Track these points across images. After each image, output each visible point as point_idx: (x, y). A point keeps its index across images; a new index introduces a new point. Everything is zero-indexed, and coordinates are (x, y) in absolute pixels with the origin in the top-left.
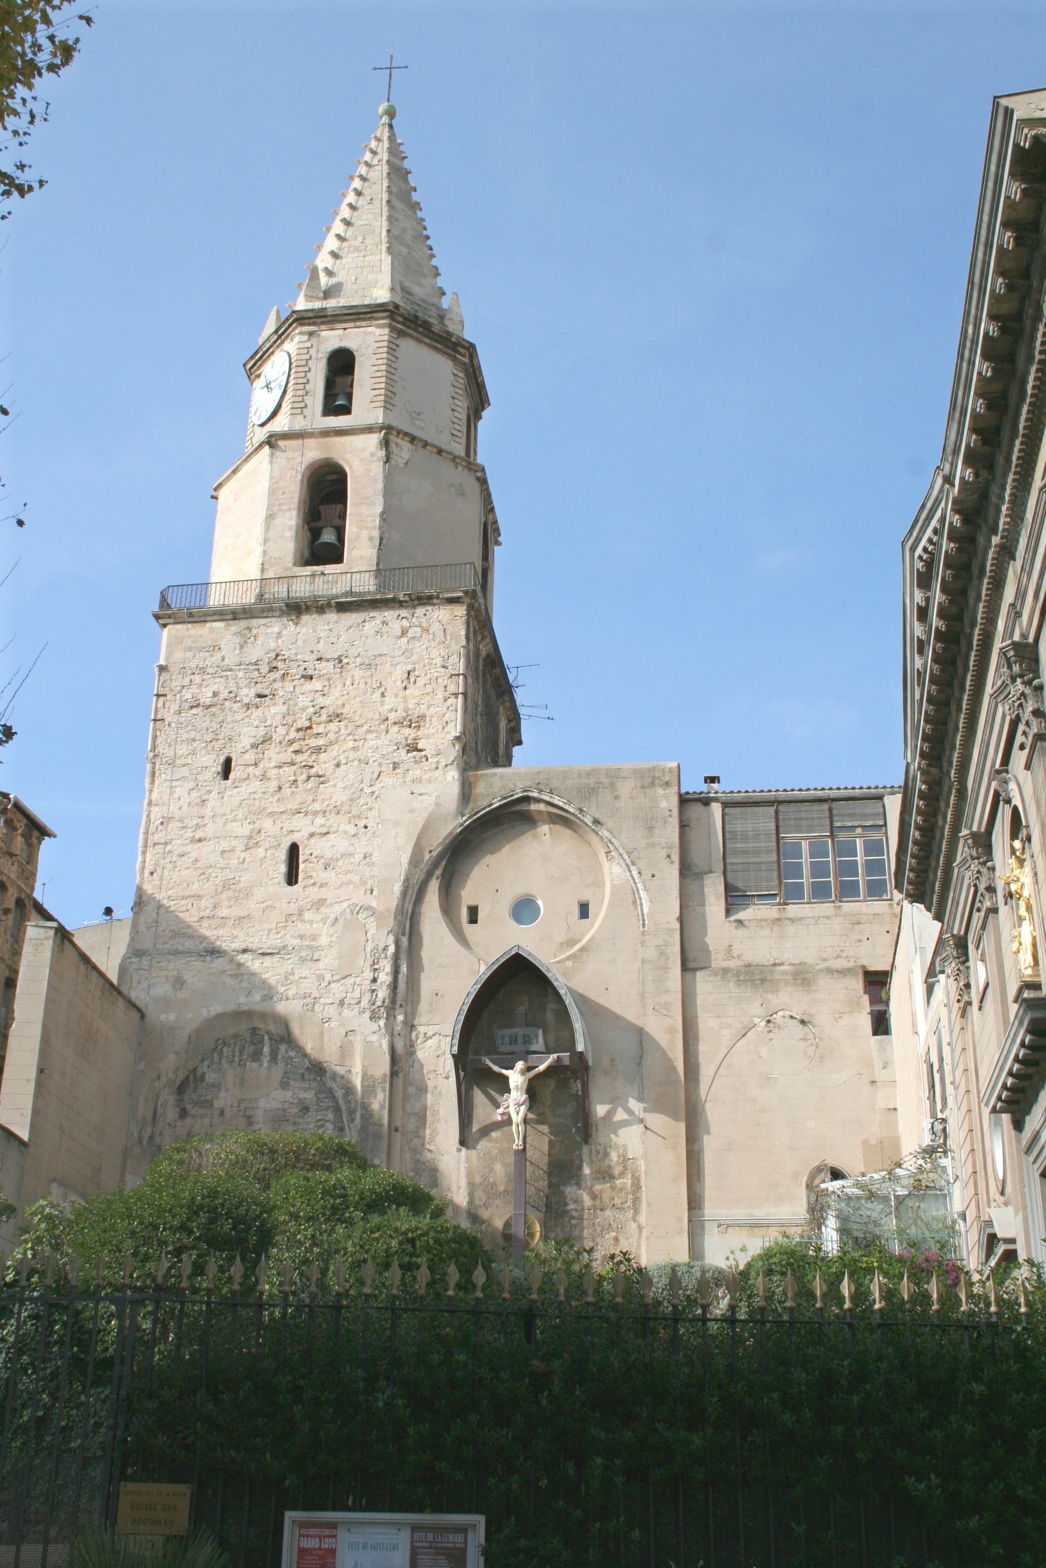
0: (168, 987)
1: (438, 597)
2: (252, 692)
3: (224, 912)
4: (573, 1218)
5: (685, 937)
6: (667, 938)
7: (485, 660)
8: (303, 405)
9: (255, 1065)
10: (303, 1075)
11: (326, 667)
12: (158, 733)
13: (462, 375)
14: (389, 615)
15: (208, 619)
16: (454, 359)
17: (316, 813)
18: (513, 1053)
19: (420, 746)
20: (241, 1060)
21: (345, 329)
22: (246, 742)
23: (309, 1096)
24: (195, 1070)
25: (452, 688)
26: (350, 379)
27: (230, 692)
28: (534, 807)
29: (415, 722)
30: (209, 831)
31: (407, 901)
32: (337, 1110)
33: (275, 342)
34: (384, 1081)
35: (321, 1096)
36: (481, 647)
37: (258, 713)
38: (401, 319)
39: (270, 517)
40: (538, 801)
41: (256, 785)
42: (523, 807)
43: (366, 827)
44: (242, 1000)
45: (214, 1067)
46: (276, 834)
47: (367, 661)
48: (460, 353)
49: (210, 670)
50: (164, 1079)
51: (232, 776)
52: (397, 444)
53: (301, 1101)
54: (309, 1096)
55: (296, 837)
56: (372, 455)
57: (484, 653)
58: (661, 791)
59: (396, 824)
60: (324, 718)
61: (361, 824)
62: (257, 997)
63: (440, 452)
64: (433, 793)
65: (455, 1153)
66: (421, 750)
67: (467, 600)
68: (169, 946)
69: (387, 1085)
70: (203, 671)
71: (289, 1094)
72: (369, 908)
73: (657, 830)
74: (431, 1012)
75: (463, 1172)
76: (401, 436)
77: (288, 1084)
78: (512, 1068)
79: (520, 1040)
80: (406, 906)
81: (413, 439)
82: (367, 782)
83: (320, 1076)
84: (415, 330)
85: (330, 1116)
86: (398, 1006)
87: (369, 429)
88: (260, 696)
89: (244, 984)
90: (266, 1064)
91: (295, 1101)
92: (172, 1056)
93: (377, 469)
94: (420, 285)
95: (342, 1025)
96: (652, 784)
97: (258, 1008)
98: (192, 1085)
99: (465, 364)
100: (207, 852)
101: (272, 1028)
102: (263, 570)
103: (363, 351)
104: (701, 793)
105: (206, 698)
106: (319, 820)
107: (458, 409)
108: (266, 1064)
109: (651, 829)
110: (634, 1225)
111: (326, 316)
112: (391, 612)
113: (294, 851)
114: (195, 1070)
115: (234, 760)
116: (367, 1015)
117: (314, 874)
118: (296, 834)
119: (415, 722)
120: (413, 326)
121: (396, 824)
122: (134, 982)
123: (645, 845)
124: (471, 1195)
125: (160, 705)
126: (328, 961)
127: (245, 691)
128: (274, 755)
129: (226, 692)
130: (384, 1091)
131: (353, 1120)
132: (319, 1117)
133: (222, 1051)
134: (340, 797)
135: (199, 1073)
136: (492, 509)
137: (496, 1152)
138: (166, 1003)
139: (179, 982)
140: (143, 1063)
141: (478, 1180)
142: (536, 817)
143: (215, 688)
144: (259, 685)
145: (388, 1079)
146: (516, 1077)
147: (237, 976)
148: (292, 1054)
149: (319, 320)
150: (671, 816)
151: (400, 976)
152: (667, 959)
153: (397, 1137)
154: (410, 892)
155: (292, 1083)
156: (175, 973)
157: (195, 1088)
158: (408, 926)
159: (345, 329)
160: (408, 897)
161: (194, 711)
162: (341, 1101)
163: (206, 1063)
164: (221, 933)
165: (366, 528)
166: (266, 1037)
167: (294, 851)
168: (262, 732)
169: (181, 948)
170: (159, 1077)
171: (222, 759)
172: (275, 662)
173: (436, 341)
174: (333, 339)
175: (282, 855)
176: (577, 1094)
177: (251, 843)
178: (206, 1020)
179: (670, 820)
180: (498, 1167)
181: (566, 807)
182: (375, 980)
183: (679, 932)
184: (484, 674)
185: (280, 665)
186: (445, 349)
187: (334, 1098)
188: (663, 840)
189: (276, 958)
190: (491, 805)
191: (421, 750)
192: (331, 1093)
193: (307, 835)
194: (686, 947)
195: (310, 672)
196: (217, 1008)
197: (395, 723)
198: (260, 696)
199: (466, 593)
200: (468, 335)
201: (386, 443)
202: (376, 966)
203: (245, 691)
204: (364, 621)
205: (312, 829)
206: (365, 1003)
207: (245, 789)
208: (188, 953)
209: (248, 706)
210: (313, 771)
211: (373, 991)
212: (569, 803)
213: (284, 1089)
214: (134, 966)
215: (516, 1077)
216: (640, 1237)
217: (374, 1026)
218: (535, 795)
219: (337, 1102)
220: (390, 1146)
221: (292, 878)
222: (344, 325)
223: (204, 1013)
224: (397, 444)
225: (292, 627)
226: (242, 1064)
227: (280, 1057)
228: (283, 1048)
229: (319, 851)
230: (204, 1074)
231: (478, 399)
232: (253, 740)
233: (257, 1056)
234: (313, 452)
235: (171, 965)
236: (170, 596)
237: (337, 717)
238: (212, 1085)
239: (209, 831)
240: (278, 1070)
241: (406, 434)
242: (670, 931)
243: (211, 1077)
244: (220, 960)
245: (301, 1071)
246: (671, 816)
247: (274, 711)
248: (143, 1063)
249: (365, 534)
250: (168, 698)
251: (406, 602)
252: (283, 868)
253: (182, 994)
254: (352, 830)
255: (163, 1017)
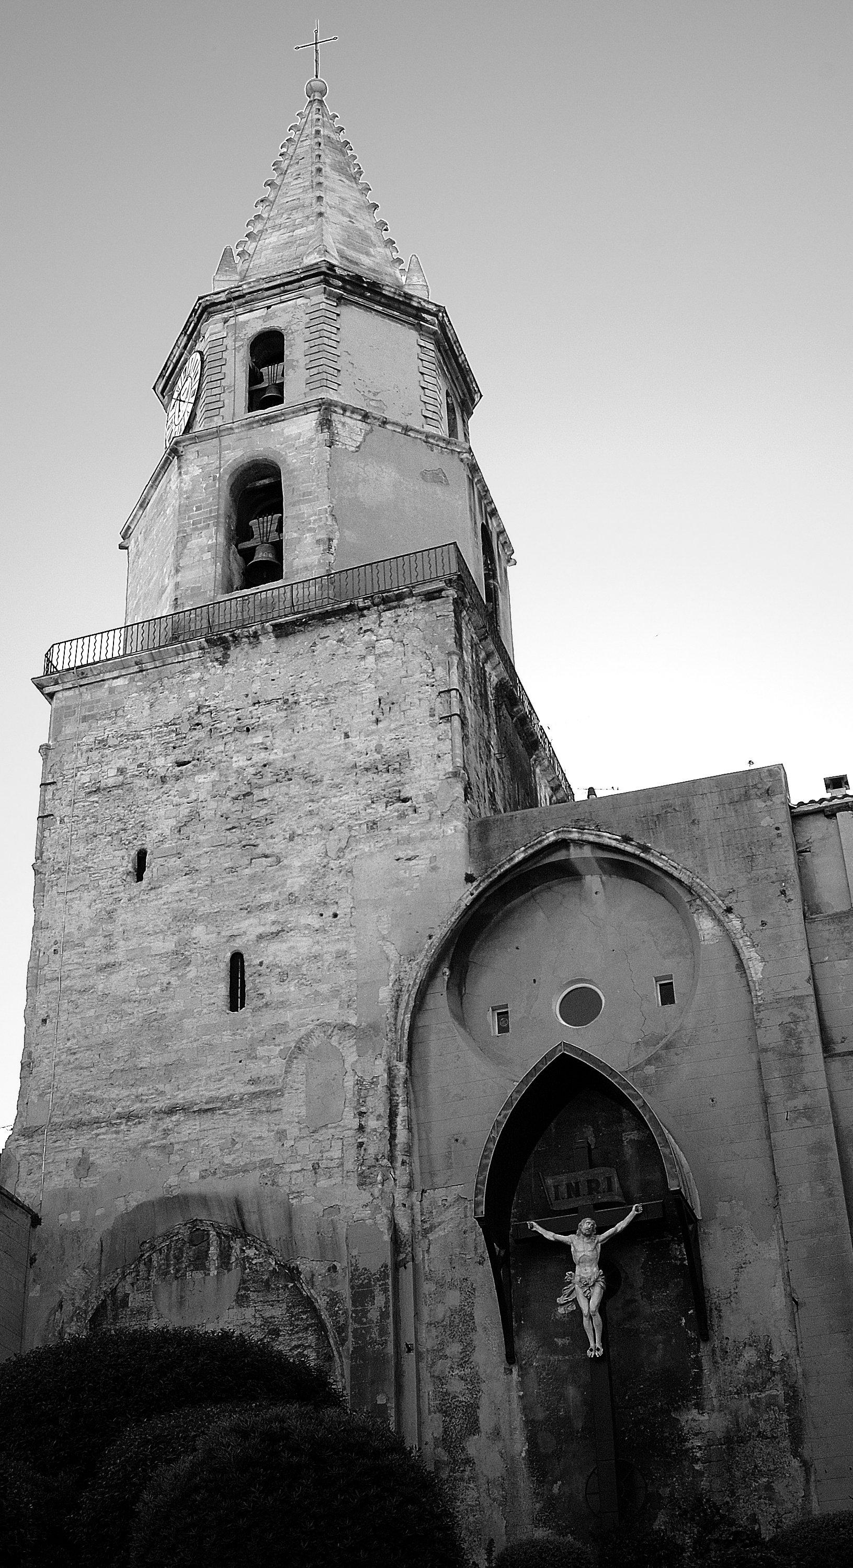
0: (69, 1175)
1: (411, 595)
2: (171, 759)
3: (144, 1061)
4: (697, 1460)
5: (824, 1008)
6: (796, 1011)
7: (496, 688)
8: (220, 404)
9: (199, 1275)
10: (267, 1284)
11: (272, 715)
12: (46, 834)
13: (432, 347)
14: (346, 628)
15: (107, 676)
16: (419, 328)
17: (262, 907)
18: (574, 1210)
19: (403, 795)
20: (178, 1271)
21: (269, 307)
22: (166, 826)
23: (278, 1312)
24: (114, 1291)
25: (441, 711)
26: (280, 366)
27: (140, 765)
28: (574, 853)
29: (395, 764)
30: (120, 955)
31: (401, 1011)
32: (321, 1327)
33: (185, 347)
34: (384, 1275)
35: (296, 1311)
36: (488, 668)
37: (179, 786)
38: (340, 284)
39: (183, 540)
40: (580, 843)
41: (182, 883)
42: (560, 856)
43: (335, 915)
44: (173, 1180)
45: (140, 1283)
46: (210, 943)
47: (322, 695)
48: (426, 321)
49: (110, 743)
50: (68, 1308)
51: (146, 874)
52: (344, 424)
53: (266, 1321)
54: (278, 1312)
55: (237, 945)
56: (311, 440)
57: (494, 680)
58: (760, 804)
59: (378, 904)
60: (269, 778)
61: (328, 913)
62: (195, 1175)
63: (406, 430)
64: (436, 866)
65: (503, 1377)
66: (405, 800)
67: (452, 592)
68: (67, 1118)
69: (390, 1281)
70: (103, 743)
71: (249, 1312)
72: (344, 1027)
73: (761, 858)
74: (449, 1167)
75: (516, 1405)
76: (348, 414)
77: (247, 1297)
78: (571, 1230)
79: (584, 1189)
80: (401, 1018)
81: (366, 416)
82: (332, 854)
83: (293, 1281)
84: (362, 296)
85: (311, 1339)
86: (399, 1164)
87: (305, 409)
88: (180, 764)
89: (175, 1158)
90: (214, 1272)
91: (259, 1323)
92: (77, 1273)
93: (319, 453)
94: (368, 254)
95: (318, 1200)
96: (747, 796)
97: (194, 1189)
98: (110, 1314)
99: (435, 333)
100: (118, 983)
101: (218, 1217)
102: (176, 606)
103: (294, 327)
104: (822, 800)
105: (110, 777)
106: (271, 916)
107: (430, 387)
108: (214, 1272)
109: (752, 858)
110: (796, 1463)
111: (243, 296)
112: (349, 625)
113: (237, 960)
114: (114, 1291)
115: (149, 852)
116: (354, 1180)
117: (267, 991)
118: (238, 940)
119: (395, 764)
120: (358, 291)
121: (378, 904)
122: (23, 1173)
123: (744, 883)
124: (532, 1440)
125: (49, 796)
126: (294, 1106)
127: (160, 761)
128: (205, 836)
129: (134, 766)
130: (385, 1291)
131: (343, 1341)
132: (294, 1343)
133: (150, 1260)
134: (296, 882)
135: (119, 1295)
136: (494, 513)
137: (565, 1367)
138: (68, 1198)
139: (84, 1166)
140: (38, 1287)
141: (540, 1415)
142: (581, 868)
143: (121, 763)
144: (177, 751)
145: (390, 1272)
146: (583, 1248)
147: (164, 1147)
148: (251, 1252)
149: (234, 303)
150: (779, 836)
151: (399, 1119)
152: (799, 1042)
153: (410, 1360)
154: (405, 997)
155: (253, 1296)
156: (78, 1153)
157: (115, 1317)
158: (405, 1047)
159: (269, 307)
160: (403, 1005)
161: (94, 798)
162: (325, 1315)
163: (129, 1279)
164: (140, 1090)
165: (310, 530)
166: (213, 1233)
167: (237, 960)
168: (184, 811)
169: (86, 1118)
170: (61, 1306)
171: (134, 853)
172: (200, 717)
173: (389, 307)
174: (253, 321)
175: (223, 968)
176: (682, 1265)
177: (180, 958)
178: (122, 1216)
179: (779, 841)
180: (571, 1392)
181: (622, 846)
182: (361, 1128)
183: (813, 999)
184: (497, 708)
185: (204, 719)
186: (404, 317)
187: (315, 1312)
188: (772, 872)
189: (218, 1115)
190: (512, 859)
191: (405, 800)
192: (309, 1303)
193: (253, 937)
194: (828, 1022)
195: (246, 722)
196: (137, 1197)
197: (367, 770)
198: (180, 764)
199: (449, 582)
200: (436, 297)
201: (326, 423)
202: (363, 1109)
203: (160, 761)
204: (315, 644)
205: (261, 930)
206: (350, 1165)
207: (170, 889)
208: (96, 1122)
209: (163, 780)
210: (259, 850)
211: (361, 1145)
212: (626, 839)
213: (241, 1306)
214: (23, 1151)
215: (583, 1248)
216: (807, 1481)
217: (365, 1197)
218: (575, 836)
219: (319, 1317)
220: (399, 1374)
221: (236, 999)
222: (268, 302)
223: (121, 1206)
224: (344, 424)
225: (218, 669)
226: (179, 1276)
227: (233, 1259)
228: (236, 1245)
229: (271, 958)
230: (127, 1295)
231: (463, 394)
232: (173, 822)
233: (200, 1262)
234: (237, 452)
235: (73, 1144)
236: (55, 656)
237: (286, 775)
238: (139, 1312)
239: (120, 955)
240: (232, 1278)
241: (354, 411)
242: (799, 1001)
243: (136, 1300)
244: (140, 1127)
245: (265, 1277)
246: (779, 836)
247: (203, 782)
248: (38, 1287)
249: (308, 538)
250: (59, 785)
251: (368, 608)
252: (223, 989)
253: (89, 1183)
254: (316, 922)
255: (63, 1218)
